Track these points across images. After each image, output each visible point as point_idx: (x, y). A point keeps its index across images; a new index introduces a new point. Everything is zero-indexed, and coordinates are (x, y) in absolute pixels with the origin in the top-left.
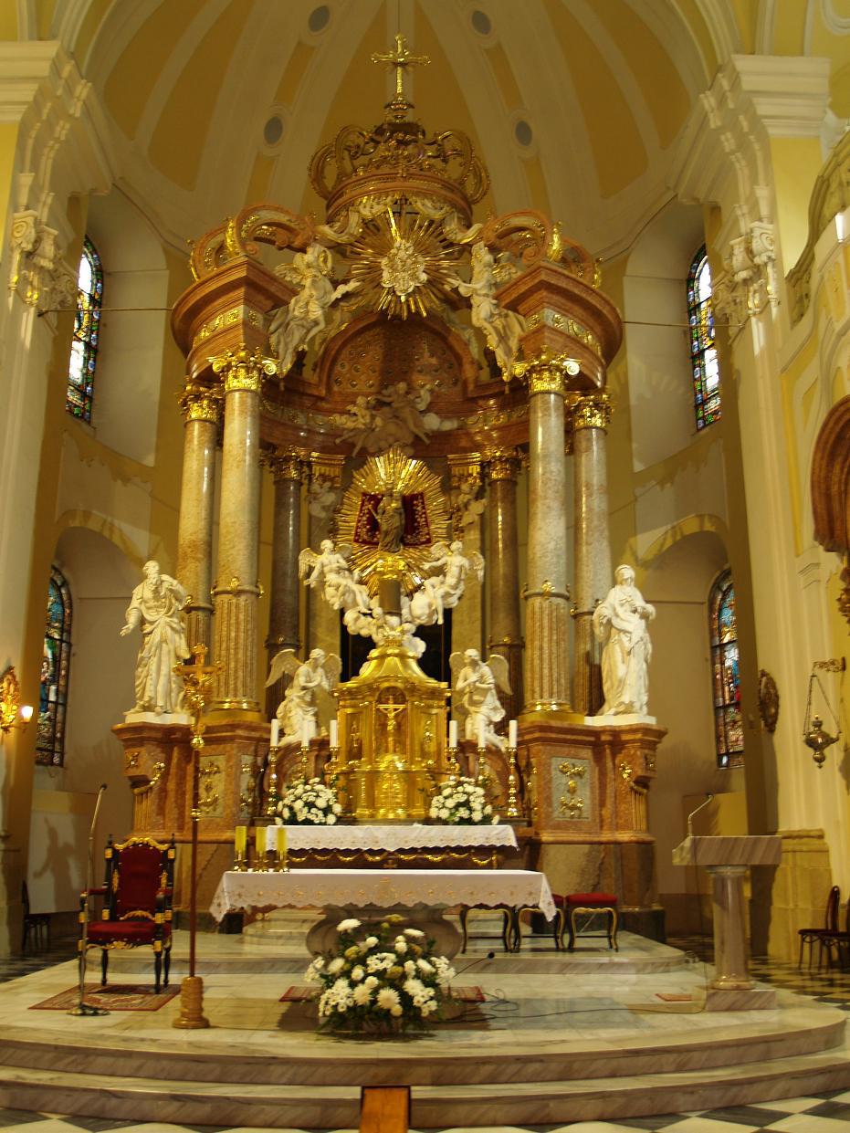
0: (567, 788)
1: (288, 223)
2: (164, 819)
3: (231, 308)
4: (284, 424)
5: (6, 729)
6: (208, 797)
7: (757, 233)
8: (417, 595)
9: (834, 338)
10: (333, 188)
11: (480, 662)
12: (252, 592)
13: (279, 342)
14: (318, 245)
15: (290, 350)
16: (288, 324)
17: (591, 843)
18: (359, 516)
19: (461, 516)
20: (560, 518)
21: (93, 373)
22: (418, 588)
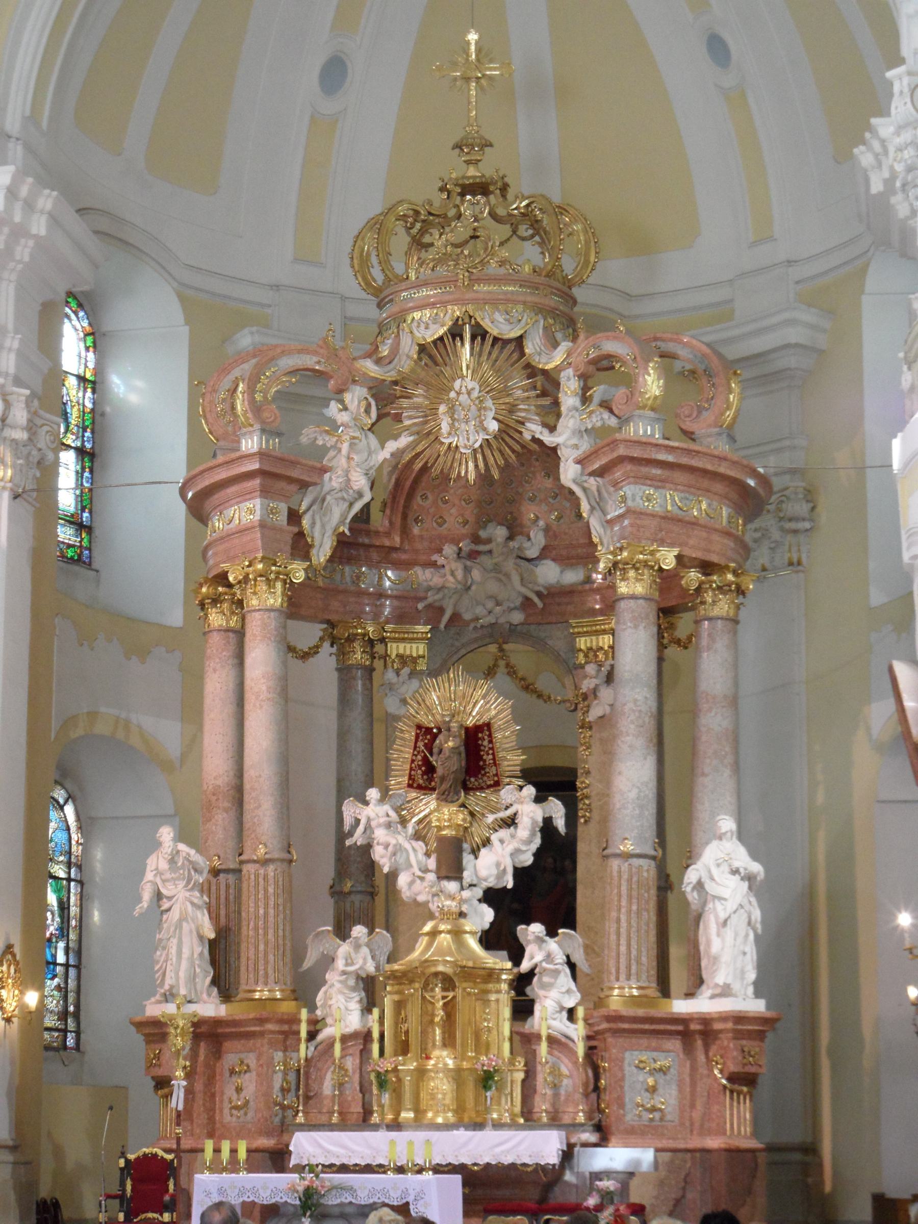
0: (646, 1087)
2: (192, 1123)
3: (246, 500)
4: (345, 592)
5: (8, 1020)
6: (239, 1099)
8: (483, 852)
11: (547, 938)
12: (282, 860)
13: (313, 524)
14: (358, 388)
15: (329, 532)
16: (324, 500)
17: (674, 1151)
18: (414, 755)
19: (588, 706)
20: (645, 759)
21: (91, 490)
22: (487, 842)
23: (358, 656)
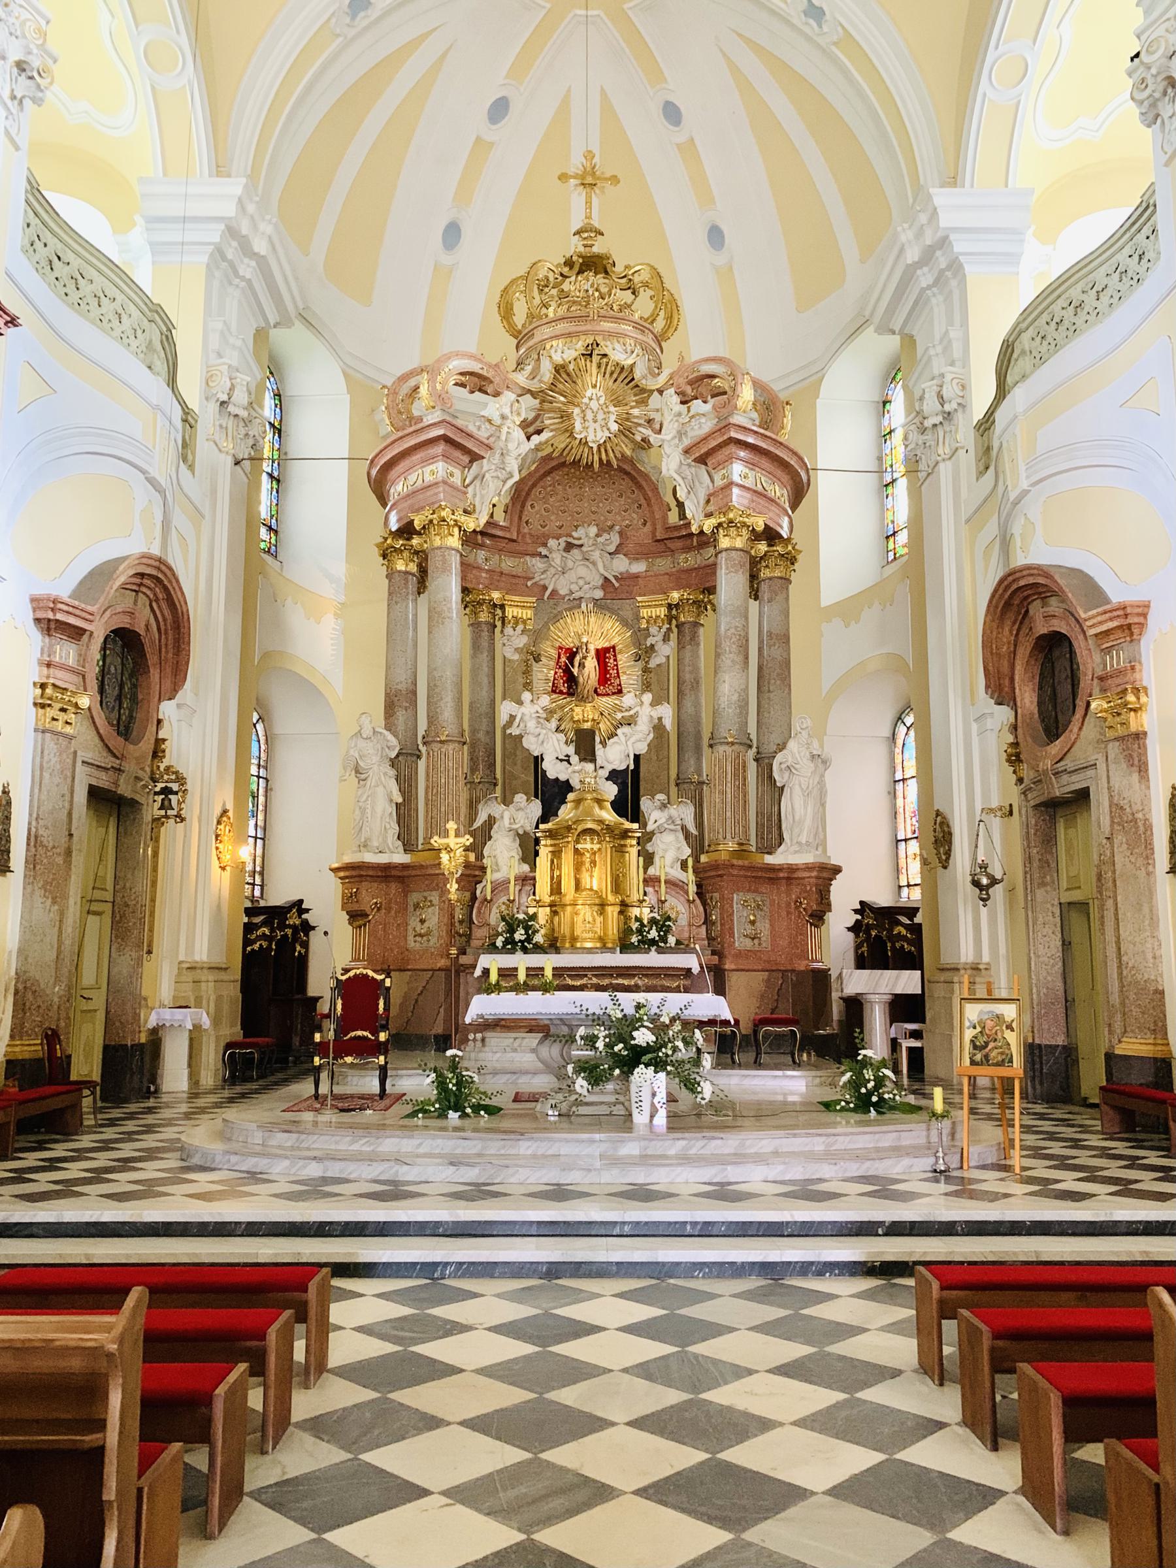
1: (481, 372)
7: (948, 377)
9: (1009, 505)
10: (524, 326)
12: (459, 742)
13: (475, 495)
23: (484, 617)
